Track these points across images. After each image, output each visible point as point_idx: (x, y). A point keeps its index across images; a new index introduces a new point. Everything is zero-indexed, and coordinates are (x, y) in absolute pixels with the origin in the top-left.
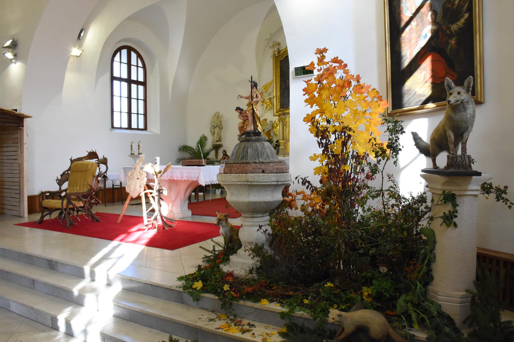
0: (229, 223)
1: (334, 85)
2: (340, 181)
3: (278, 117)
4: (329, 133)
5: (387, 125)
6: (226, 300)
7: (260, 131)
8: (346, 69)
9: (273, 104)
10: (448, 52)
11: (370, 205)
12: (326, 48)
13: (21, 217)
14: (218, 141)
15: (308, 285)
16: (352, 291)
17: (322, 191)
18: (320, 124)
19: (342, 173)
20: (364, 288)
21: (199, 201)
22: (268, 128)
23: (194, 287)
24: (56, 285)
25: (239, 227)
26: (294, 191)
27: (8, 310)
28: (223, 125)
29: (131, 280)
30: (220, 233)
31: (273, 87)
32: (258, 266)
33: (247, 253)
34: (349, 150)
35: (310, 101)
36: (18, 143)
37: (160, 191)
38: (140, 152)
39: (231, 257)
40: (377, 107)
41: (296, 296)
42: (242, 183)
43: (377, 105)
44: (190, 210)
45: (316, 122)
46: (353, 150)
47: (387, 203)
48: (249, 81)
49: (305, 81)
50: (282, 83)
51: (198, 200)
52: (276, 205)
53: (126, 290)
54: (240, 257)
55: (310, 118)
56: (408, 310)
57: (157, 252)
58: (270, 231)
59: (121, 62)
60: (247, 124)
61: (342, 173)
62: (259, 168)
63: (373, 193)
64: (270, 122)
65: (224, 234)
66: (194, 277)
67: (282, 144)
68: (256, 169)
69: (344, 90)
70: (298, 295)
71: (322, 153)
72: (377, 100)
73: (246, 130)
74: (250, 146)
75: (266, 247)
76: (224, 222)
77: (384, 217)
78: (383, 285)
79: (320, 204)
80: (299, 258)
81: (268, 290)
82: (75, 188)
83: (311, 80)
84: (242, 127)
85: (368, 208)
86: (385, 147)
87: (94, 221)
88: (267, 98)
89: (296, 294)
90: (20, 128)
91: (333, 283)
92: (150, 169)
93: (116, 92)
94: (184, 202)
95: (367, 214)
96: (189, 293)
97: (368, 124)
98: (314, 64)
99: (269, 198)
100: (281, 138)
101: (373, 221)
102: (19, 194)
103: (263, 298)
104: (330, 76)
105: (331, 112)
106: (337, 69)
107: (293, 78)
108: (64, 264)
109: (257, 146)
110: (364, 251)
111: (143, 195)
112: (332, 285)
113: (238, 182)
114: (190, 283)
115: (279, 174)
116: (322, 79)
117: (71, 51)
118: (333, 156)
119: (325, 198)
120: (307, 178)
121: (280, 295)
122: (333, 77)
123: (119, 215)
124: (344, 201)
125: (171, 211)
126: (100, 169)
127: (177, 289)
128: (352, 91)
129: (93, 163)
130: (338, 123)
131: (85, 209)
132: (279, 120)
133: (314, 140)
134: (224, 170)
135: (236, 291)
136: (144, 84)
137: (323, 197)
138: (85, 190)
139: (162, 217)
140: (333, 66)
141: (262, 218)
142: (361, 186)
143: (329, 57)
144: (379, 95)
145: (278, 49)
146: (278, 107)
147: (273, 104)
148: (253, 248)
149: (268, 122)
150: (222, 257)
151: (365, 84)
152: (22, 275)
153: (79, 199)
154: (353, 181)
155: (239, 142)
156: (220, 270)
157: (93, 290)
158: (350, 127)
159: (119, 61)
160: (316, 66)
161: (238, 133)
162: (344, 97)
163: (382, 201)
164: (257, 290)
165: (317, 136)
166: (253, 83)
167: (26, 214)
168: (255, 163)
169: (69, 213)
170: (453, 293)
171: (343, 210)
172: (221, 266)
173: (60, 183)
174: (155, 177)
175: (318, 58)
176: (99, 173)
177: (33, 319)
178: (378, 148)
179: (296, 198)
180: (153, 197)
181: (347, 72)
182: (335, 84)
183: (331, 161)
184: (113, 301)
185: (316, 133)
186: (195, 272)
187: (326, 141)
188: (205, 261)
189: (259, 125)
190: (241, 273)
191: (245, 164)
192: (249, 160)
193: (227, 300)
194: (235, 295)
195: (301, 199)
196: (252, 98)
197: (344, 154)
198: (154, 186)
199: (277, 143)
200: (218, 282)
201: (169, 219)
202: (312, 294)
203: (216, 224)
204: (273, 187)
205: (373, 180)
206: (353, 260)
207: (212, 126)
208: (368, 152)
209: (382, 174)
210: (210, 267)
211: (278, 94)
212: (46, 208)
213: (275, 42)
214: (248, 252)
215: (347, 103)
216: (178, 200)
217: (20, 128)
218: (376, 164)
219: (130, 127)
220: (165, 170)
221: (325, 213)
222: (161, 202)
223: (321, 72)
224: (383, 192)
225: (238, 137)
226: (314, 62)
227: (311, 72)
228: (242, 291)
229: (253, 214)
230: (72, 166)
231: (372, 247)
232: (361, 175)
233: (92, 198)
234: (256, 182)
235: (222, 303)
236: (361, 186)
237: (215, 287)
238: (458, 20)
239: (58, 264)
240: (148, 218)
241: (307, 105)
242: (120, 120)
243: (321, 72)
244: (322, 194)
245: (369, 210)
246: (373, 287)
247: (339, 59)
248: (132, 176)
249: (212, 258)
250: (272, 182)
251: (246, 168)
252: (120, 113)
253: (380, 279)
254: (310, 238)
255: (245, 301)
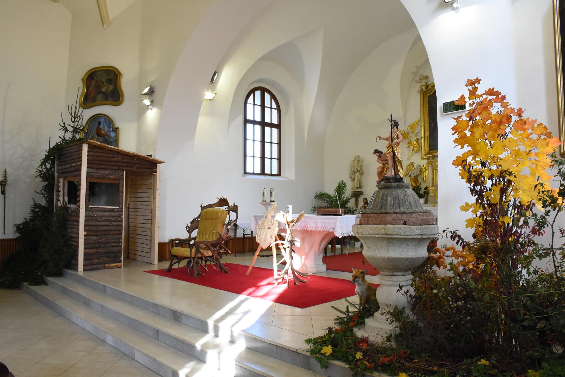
0: (366, 281)
1: (489, 122)
2: (497, 236)
3: (426, 160)
4: (484, 178)
5: (557, 168)
6: (358, 370)
7: (402, 177)
8: (504, 101)
9: (420, 146)
11: (536, 267)
12: (479, 78)
13: (151, 264)
14: (359, 187)
15: (456, 360)
16: (514, 373)
17: (476, 247)
18: (473, 167)
19: (501, 226)
20: (530, 371)
21: (336, 254)
22: (415, 173)
23: (323, 351)
24: (179, 337)
25: (378, 286)
26: (443, 247)
27: (133, 359)
28: (364, 170)
29: (255, 339)
30: (356, 291)
31: (421, 127)
32: (397, 333)
33: (384, 317)
34: (509, 198)
35: (461, 141)
36: (151, 189)
37: (292, 242)
38: (273, 199)
39: (366, 320)
40: (545, 145)
41: (442, 372)
42: (380, 236)
43: (545, 143)
44: (325, 264)
45: (468, 166)
46: (515, 199)
47: (561, 265)
48: (389, 120)
49: (454, 118)
50: (431, 122)
51: (335, 254)
52: (421, 262)
53: (250, 350)
54: (377, 321)
55: (461, 160)
57: (288, 310)
58: (412, 292)
59: (254, 104)
60: (386, 169)
61: (501, 226)
62: (400, 219)
63: (541, 252)
64: (417, 166)
65: (360, 293)
66: (323, 341)
67: (431, 192)
68: (397, 220)
69: (502, 127)
70: (444, 371)
71: (475, 202)
72: (545, 137)
73: (385, 176)
74: (390, 193)
75: (407, 311)
76: (360, 279)
77: (556, 282)
78: (557, 370)
79: (473, 263)
80: (446, 326)
81: (408, 362)
82: (204, 236)
83: (462, 116)
84: (381, 172)
85: (534, 269)
86: (556, 195)
87: (222, 272)
88: (413, 138)
89: (441, 370)
90: (154, 173)
91: (489, 361)
92: (282, 218)
93: (249, 136)
94: (319, 255)
95: (533, 277)
96: (317, 358)
97: (534, 166)
98: (465, 98)
99: (411, 253)
100: (430, 184)
101: (542, 287)
102: (151, 240)
103: (402, 372)
104: (484, 111)
105: (486, 153)
106: (493, 102)
107: (442, 115)
108: (188, 316)
109: (398, 194)
110: (530, 324)
111: (273, 245)
112: (487, 363)
113: (376, 234)
114: (319, 347)
115: (423, 227)
116: (475, 114)
117: (204, 95)
118: (490, 205)
119: (479, 256)
120: (457, 232)
121: (421, 370)
122: (487, 112)
123: (248, 267)
124: (503, 260)
125: (304, 265)
126: (230, 216)
127: (304, 353)
128: (512, 128)
129: (223, 210)
130: (495, 166)
131: (214, 259)
132: (428, 164)
133: (466, 186)
134: (360, 220)
135: (370, 360)
136: (278, 126)
137: (476, 255)
138: (214, 238)
139: (293, 271)
140: (488, 100)
141: (403, 277)
142: (525, 243)
143: (482, 89)
144: (548, 131)
145: (426, 83)
146: (427, 149)
147: (420, 146)
148: (392, 311)
149: (415, 166)
150: (356, 320)
151: (528, 118)
152: (147, 324)
153: (207, 248)
154: (514, 236)
155: (377, 189)
156: (353, 335)
157: (216, 346)
158: (510, 171)
159: (253, 103)
160: (467, 100)
161: (377, 179)
162: (502, 135)
163: (553, 262)
164: (395, 361)
165: (469, 181)
166: (393, 122)
167: (156, 262)
168: (395, 213)
169: (197, 263)
171: (502, 271)
172: (355, 330)
173: (190, 230)
174: (287, 226)
175: (470, 91)
176: (228, 221)
177: (155, 371)
178: (547, 196)
179: (445, 254)
180: (285, 249)
181: (505, 106)
182: (491, 120)
183: (486, 212)
184: (236, 361)
185: (468, 179)
186: (325, 335)
187: (481, 188)
188: (337, 323)
189: (401, 170)
190: (377, 340)
191: (384, 214)
192: (388, 210)
193: (360, 371)
194: (368, 365)
195: (450, 256)
196: (392, 139)
197: (503, 203)
198: (285, 236)
199: (425, 191)
200: (350, 349)
201: (301, 273)
202: (461, 372)
203: (351, 282)
204: (420, 240)
205: (541, 235)
206: (514, 334)
207: (352, 171)
208: (534, 201)
209: (552, 228)
210: (342, 330)
211: (427, 134)
212: (175, 256)
213: (423, 75)
214: (386, 316)
215: (506, 142)
216: (312, 252)
217: (154, 173)
218: (544, 215)
219: (263, 173)
220: (298, 220)
221: (480, 274)
222: (293, 254)
223: (474, 106)
224: (553, 251)
225: (376, 184)
226: (465, 96)
227: (463, 107)
228: (377, 361)
229: (393, 272)
230: (202, 213)
231: (540, 319)
232: (525, 229)
233: (221, 247)
234: (396, 235)
235: (353, 373)
236: (525, 243)
237: (346, 354)
239: (182, 316)
240: (279, 271)
241: (457, 146)
242: (254, 165)
243: (474, 106)
244: (476, 251)
245: (536, 272)
246: (543, 371)
247: (495, 90)
248: (263, 225)
249: (345, 320)
250: (415, 235)
251: (385, 219)
252: (252, 157)
253: (552, 362)
254: (460, 303)
255: (380, 373)
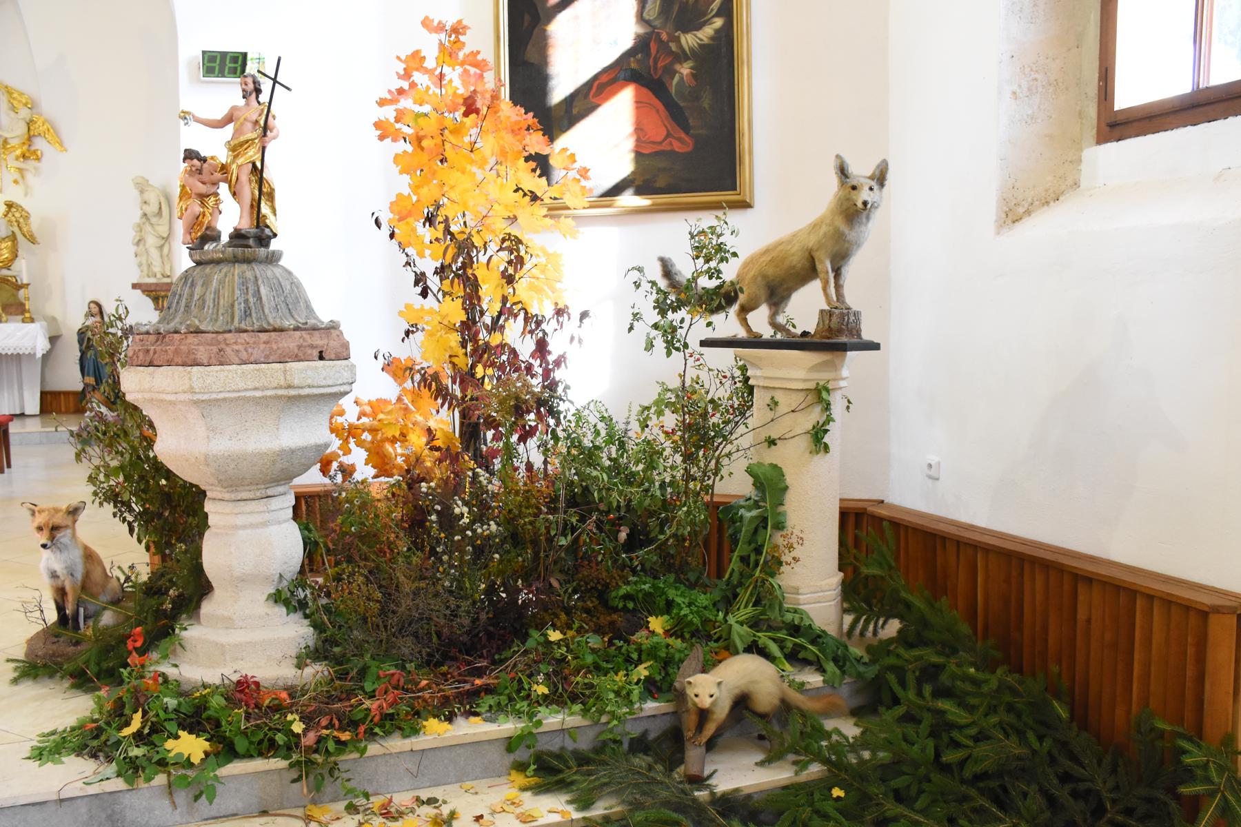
10: (673, 92)
42: (269, 393)
56: (757, 641)
62: (312, 347)
113: (256, 389)
170: (823, 583)
175: (441, 44)
229: (267, 488)
238: (699, 28)
